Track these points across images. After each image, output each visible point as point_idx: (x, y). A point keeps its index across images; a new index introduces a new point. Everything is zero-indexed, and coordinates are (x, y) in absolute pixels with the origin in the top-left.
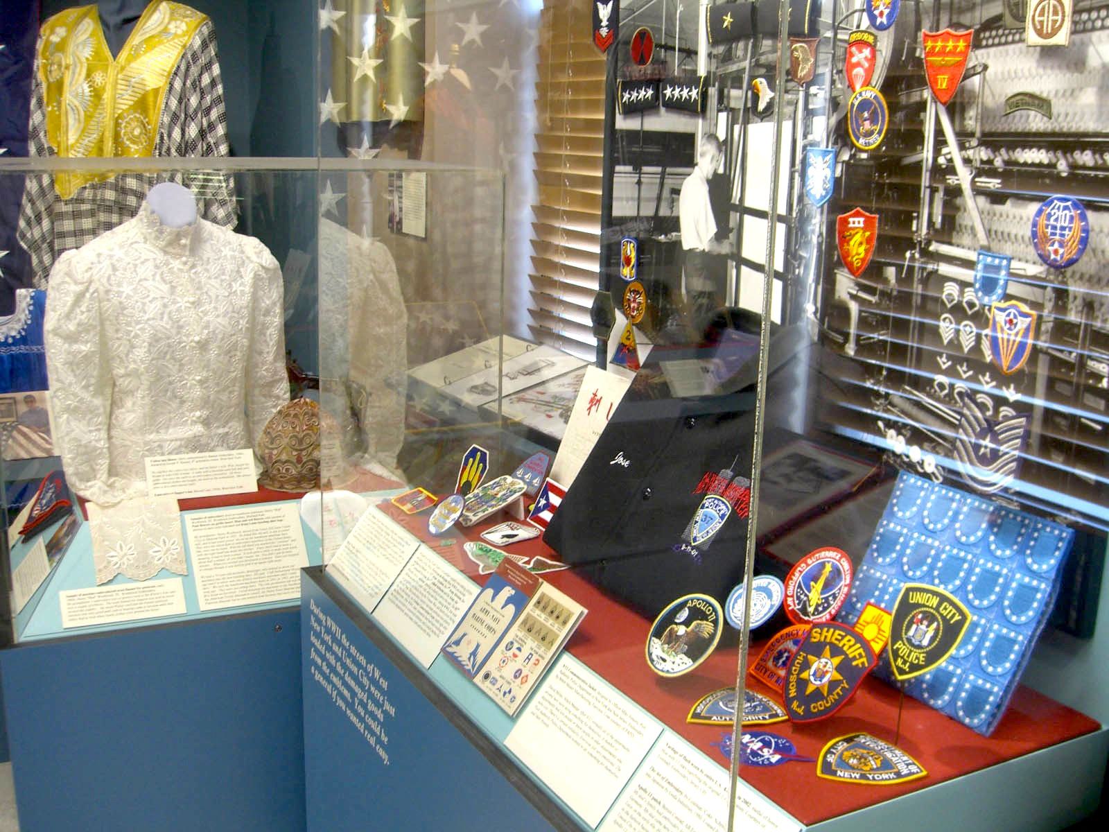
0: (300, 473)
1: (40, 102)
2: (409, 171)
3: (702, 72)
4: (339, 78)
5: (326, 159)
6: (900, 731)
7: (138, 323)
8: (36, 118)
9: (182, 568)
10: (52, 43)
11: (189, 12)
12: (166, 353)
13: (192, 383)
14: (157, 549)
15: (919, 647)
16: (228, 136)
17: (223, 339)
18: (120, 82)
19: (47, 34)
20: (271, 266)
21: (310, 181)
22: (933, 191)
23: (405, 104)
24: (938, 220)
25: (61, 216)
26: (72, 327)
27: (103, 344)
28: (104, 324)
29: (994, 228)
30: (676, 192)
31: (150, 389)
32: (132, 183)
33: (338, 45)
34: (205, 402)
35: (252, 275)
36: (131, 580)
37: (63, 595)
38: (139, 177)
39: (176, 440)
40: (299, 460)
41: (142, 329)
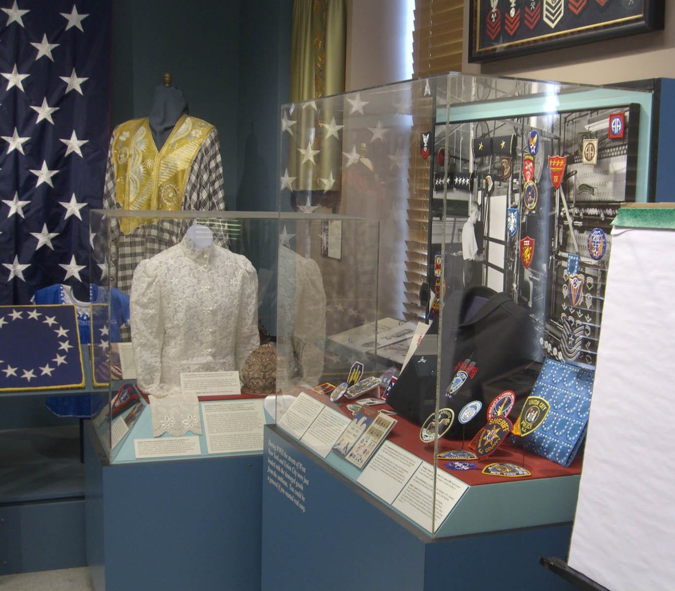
0: (264, 385)
1: (112, 176)
2: (332, 220)
3: (471, 171)
4: (292, 162)
5: (282, 213)
6: (525, 463)
7: (180, 299)
8: (109, 185)
9: (199, 431)
10: (120, 141)
11: (203, 124)
12: (194, 316)
13: (207, 333)
14: (186, 420)
15: (530, 422)
16: (225, 198)
17: (225, 310)
18: (162, 165)
19: (118, 135)
20: (252, 271)
21: (274, 227)
22: (559, 228)
23: (334, 179)
24: (561, 241)
25: (123, 245)
26: (145, 300)
27: (161, 311)
28: (161, 300)
29: (580, 244)
30: (461, 230)
31: (185, 335)
32: (167, 225)
33: (292, 142)
34: (214, 344)
35: (241, 276)
36: (172, 436)
37: (136, 441)
38: (171, 222)
39: (197, 364)
40: (264, 377)
41: (182, 303)
